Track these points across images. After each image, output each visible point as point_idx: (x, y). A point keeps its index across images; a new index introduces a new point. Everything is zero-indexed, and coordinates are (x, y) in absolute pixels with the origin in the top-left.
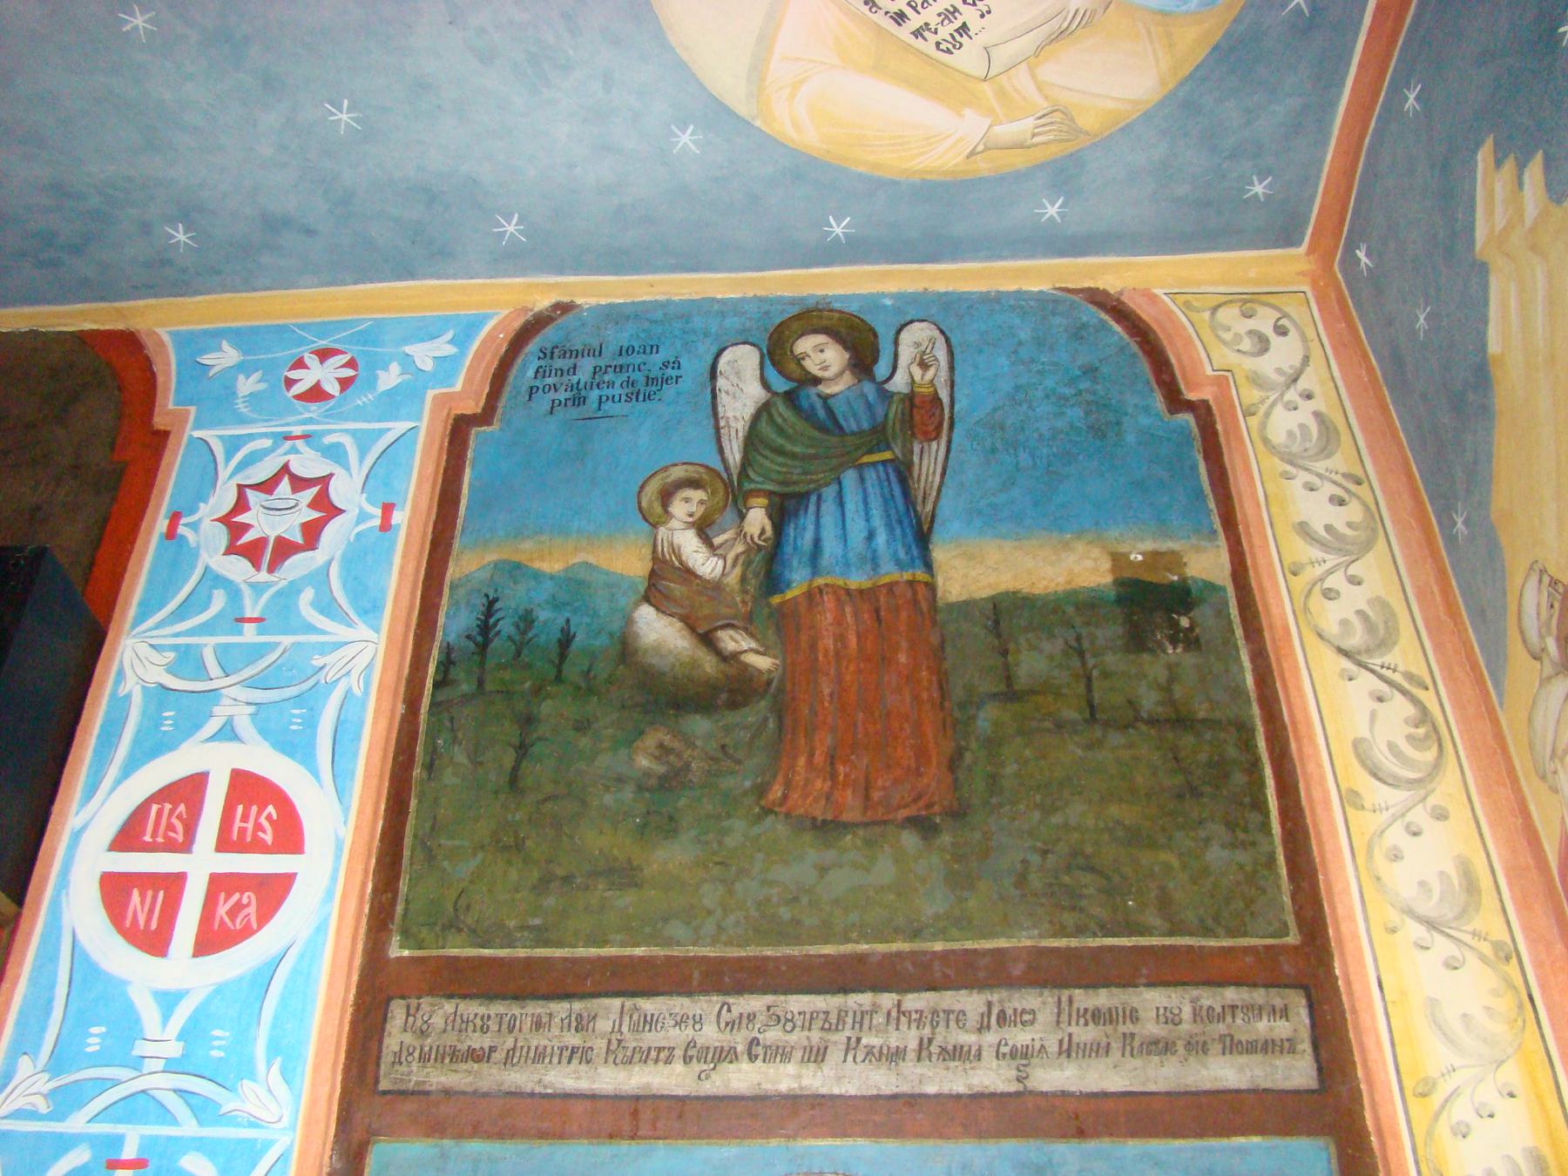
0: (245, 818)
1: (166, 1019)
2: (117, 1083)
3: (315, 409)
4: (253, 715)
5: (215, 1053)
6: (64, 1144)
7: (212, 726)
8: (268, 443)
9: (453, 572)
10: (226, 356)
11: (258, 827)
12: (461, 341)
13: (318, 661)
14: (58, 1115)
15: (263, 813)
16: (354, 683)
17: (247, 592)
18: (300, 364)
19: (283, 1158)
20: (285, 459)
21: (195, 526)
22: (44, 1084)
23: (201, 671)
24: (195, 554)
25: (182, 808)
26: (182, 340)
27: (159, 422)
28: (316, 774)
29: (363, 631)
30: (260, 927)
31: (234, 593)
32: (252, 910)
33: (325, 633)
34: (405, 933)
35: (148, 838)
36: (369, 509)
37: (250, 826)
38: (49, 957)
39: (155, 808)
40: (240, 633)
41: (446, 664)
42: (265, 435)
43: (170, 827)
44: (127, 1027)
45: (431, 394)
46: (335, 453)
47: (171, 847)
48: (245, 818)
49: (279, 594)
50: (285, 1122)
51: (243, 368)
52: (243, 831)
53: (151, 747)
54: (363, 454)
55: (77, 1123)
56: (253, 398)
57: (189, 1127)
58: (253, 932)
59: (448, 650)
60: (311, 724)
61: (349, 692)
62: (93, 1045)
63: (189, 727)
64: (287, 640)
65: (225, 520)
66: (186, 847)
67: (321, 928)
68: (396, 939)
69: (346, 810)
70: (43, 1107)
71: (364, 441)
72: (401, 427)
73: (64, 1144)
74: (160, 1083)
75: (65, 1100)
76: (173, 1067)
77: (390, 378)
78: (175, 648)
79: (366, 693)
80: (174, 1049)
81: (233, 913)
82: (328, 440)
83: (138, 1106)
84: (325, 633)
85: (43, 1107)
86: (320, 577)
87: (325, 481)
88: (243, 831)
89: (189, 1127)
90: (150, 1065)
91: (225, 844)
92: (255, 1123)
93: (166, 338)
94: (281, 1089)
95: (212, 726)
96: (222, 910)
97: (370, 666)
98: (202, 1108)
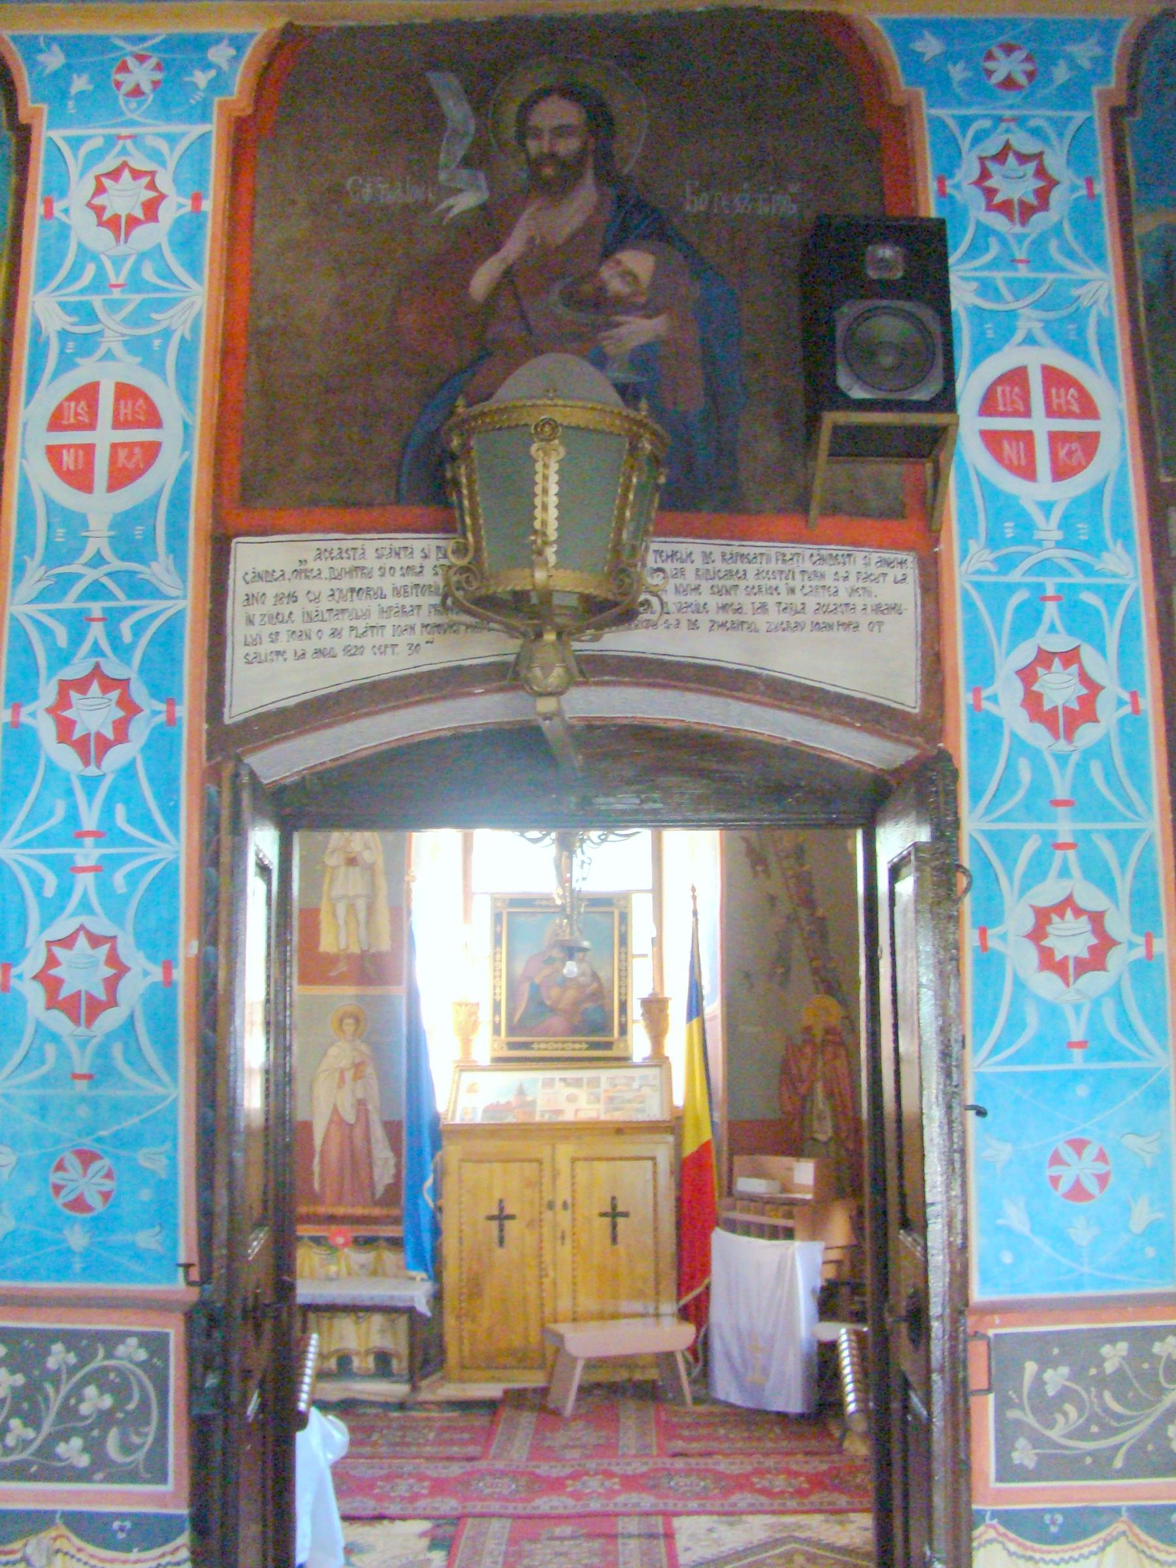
0: (1058, 397)
1: (1047, 517)
2: (1030, 554)
3: (1012, 97)
4: (1044, 328)
5: (1082, 538)
6: (1011, 588)
7: (1019, 336)
8: (987, 124)
9: (1138, 230)
10: (930, 46)
11: (1068, 403)
12: (1106, 44)
13: (1075, 293)
14: (1004, 571)
15: (136, 407)
16: (1101, 307)
17: (1012, 241)
18: (990, 57)
19: (1136, 593)
20: (1004, 138)
21: (957, 187)
22: (987, 555)
23: (999, 298)
24: (965, 210)
25: (1016, 389)
26: (896, 27)
27: (897, 100)
28: (165, 381)
29: (1096, 273)
30: (1088, 462)
31: (1003, 242)
32: (1079, 453)
33: (1072, 272)
34: (1167, 468)
35: (1001, 408)
36: (183, 201)
37: (1062, 401)
38: (964, 481)
39: (999, 389)
40: (1016, 270)
41: (1149, 298)
42: (984, 117)
43: (1013, 402)
44: (1026, 525)
45: (1095, 89)
46: (155, 155)
47: (79, 426)
48: (1058, 397)
49: (1033, 243)
50: (1131, 575)
51: (949, 57)
52: (1059, 405)
53: (66, 364)
54: (1061, 135)
55: (1015, 576)
56: (965, 83)
57: (1079, 578)
58: (1084, 468)
59: (1148, 287)
60: (1081, 332)
61: (1100, 315)
62: (1009, 534)
63: (1006, 334)
64: (1051, 277)
65: (1053, 183)
66: (91, 426)
67: (1123, 465)
68: (1162, 471)
69: (1119, 393)
70: (992, 567)
71: (1060, 125)
72: (1080, 116)
73: (1011, 588)
74: (1057, 554)
75: (1006, 564)
76: (1059, 545)
77: (1061, 73)
78: (976, 279)
79: (1111, 313)
80: (1058, 535)
81: (1070, 454)
82: (1033, 123)
83: (1045, 566)
84: (1072, 272)
85: (992, 567)
86: (1058, 229)
87: (1040, 155)
88: (1059, 405)
89: (1079, 578)
90: (1046, 544)
91: (118, 424)
92: (1115, 576)
93: (876, 24)
94: (1126, 557)
95: (1019, 336)
96: (1062, 453)
97: (1109, 298)
98: (1085, 569)
